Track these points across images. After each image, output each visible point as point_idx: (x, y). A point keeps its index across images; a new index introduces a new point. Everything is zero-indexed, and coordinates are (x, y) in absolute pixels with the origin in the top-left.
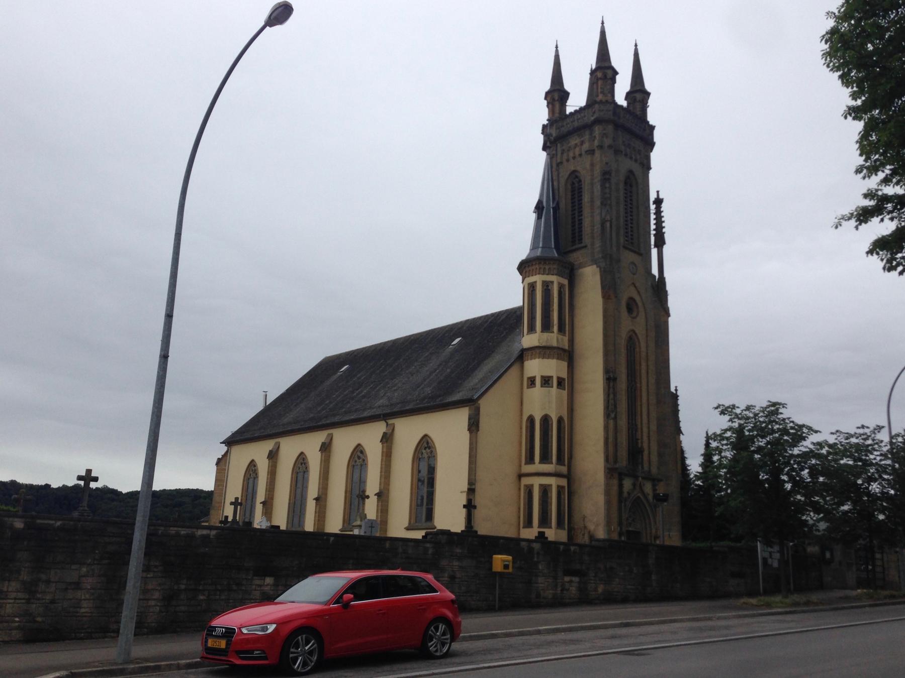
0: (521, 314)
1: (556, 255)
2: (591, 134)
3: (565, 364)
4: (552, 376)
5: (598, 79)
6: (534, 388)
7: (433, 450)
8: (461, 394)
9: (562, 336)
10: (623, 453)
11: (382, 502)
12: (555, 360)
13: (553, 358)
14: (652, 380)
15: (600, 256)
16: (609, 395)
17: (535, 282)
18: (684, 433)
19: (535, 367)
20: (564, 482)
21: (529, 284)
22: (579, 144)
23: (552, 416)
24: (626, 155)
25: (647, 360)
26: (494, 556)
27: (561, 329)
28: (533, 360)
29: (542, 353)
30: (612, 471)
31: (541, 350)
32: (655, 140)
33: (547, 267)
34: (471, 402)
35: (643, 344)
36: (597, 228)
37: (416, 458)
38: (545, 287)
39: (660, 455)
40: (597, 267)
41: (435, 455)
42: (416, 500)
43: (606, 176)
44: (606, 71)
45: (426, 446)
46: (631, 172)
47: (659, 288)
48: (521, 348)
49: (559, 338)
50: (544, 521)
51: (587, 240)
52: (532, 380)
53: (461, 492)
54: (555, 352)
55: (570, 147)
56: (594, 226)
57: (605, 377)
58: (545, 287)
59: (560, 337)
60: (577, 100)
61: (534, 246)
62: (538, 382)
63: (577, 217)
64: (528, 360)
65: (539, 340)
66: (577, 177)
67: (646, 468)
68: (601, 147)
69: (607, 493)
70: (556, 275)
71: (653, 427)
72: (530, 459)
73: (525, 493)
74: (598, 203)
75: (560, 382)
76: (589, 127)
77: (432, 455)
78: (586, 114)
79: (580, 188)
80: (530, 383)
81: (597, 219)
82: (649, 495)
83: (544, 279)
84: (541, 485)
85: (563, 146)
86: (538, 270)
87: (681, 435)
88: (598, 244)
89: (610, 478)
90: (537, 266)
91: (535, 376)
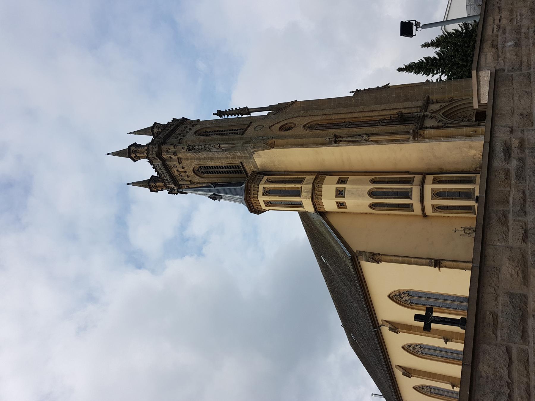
1: (244, 185)
4: (336, 188)
5: (137, 156)
10: (402, 128)
12: (323, 186)
14: (345, 110)
17: (264, 201)
20: (430, 178)
22: (176, 169)
24: (184, 136)
27: (300, 181)
28: (324, 204)
29: (317, 196)
30: (417, 136)
31: (315, 198)
33: (253, 192)
34: (355, 258)
35: (316, 118)
36: (226, 154)
38: (268, 193)
39: (406, 100)
40: (254, 154)
42: (438, 393)
43: (191, 148)
50: (467, 195)
51: (237, 163)
52: (340, 204)
54: (317, 187)
55: (180, 175)
57: (335, 145)
58: (268, 193)
59: (305, 182)
63: (212, 170)
66: (198, 170)
68: (175, 153)
69: (438, 138)
71: (383, 107)
72: (409, 207)
73: (440, 212)
75: (342, 181)
77: (408, 293)
84: (432, 198)
86: (255, 199)
88: (238, 154)
90: (252, 199)
91: (336, 202)
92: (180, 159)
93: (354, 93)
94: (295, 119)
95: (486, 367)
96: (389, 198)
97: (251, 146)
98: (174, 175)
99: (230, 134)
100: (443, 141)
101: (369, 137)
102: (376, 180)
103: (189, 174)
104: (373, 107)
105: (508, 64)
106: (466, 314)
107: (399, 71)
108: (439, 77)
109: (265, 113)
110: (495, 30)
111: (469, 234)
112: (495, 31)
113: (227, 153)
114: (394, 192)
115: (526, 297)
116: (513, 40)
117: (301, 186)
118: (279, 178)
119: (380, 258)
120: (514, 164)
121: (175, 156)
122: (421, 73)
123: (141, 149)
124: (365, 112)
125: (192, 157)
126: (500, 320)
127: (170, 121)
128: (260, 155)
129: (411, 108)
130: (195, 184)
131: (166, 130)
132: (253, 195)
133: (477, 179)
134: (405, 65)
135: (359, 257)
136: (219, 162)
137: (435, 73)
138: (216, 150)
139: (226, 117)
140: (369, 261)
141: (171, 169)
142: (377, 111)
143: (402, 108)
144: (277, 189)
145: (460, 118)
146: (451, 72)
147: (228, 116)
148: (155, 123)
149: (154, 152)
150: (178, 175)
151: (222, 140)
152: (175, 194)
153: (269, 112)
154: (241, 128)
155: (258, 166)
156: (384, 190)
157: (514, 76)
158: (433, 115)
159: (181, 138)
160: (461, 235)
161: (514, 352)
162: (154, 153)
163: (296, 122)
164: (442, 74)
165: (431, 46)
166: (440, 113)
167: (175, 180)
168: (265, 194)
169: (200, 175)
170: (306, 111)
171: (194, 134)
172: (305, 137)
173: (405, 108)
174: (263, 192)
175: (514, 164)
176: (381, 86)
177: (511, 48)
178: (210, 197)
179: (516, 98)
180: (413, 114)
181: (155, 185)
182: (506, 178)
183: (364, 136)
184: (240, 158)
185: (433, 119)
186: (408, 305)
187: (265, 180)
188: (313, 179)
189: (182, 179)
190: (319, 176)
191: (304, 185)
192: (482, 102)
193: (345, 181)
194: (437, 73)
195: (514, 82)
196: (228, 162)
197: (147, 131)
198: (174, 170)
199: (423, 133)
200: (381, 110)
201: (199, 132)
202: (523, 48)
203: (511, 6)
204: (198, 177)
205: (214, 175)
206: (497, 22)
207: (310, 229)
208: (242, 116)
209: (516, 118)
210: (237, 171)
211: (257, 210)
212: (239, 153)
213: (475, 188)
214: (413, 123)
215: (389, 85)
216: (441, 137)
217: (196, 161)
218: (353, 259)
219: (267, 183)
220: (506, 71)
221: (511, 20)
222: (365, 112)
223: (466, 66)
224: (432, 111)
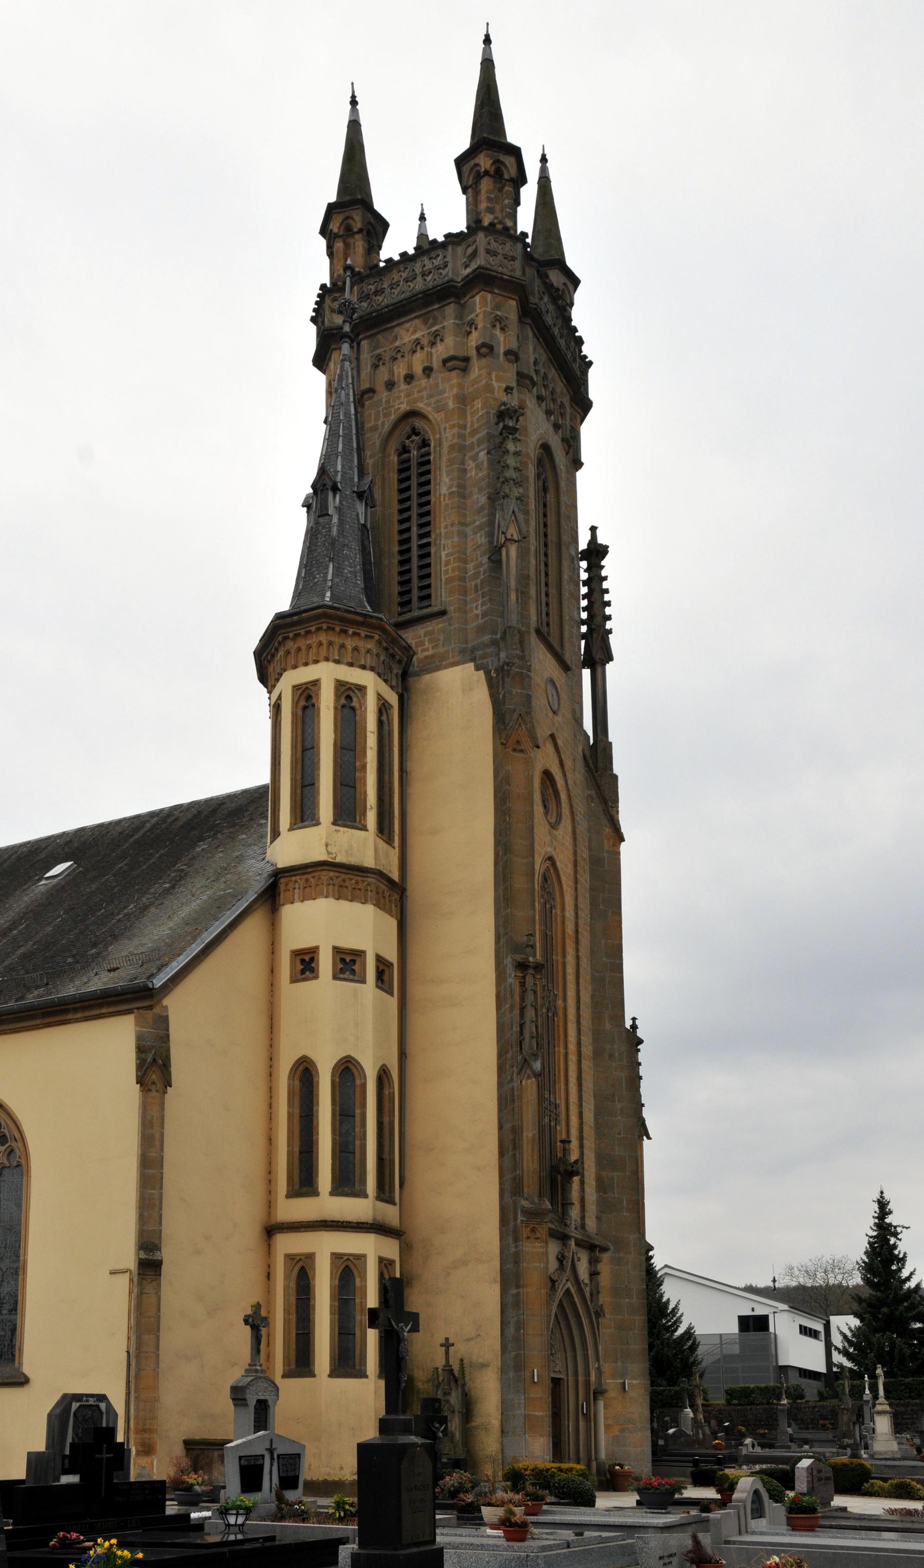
2: (460, 316)
5: (479, 177)
6: (313, 982)
7: (17, 1146)
12: (370, 909)
13: (365, 902)
17: (316, 683)
18: (651, 1134)
20: (390, 1248)
21: (296, 688)
22: (425, 341)
25: (577, 942)
26: (91, 1441)
28: (309, 903)
31: (332, 874)
32: (592, 395)
33: (350, 643)
40: (477, 668)
41: (23, 1162)
44: (503, 157)
48: (270, 869)
52: (307, 958)
53: (113, 1273)
58: (343, 701)
62: (325, 963)
63: (414, 529)
64: (292, 903)
66: (414, 431)
68: (486, 349)
70: (372, 669)
73: (287, 1277)
75: (383, 968)
78: (449, 259)
79: (425, 462)
83: (342, 677)
84: (336, 1257)
85: (376, 347)
87: (645, 1138)
91: (317, 948)
92: (462, 364)
94: (570, 828)
104: (588, 1085)
109: (588, 724)
113: (481, 565)
117: (368, 827)
118: (393, 751)
125: (469, 420)
127: (586, 350)
128: (471, 689)
132: (338, 640)
136: (446, 527)
141: (425, 322)
147: (585, 583)
150: (397, 344)
155: (427, 677)
156: (358, 1111)
166: (569, 1283)
169: (397, 432)
171: (544, 441)
174: (347, 683)
176: (645, 1113)
188: (390, 871)
190: (397, 894)
193: (382, 981)
204: (387, 427)
211: (277, 650)
212: (478, 612)
213: (367, 1377)
215: (645, 1138)
217: (455, 430)
218: (137, 995)
219: (378, 704)
224: (576, 1259)
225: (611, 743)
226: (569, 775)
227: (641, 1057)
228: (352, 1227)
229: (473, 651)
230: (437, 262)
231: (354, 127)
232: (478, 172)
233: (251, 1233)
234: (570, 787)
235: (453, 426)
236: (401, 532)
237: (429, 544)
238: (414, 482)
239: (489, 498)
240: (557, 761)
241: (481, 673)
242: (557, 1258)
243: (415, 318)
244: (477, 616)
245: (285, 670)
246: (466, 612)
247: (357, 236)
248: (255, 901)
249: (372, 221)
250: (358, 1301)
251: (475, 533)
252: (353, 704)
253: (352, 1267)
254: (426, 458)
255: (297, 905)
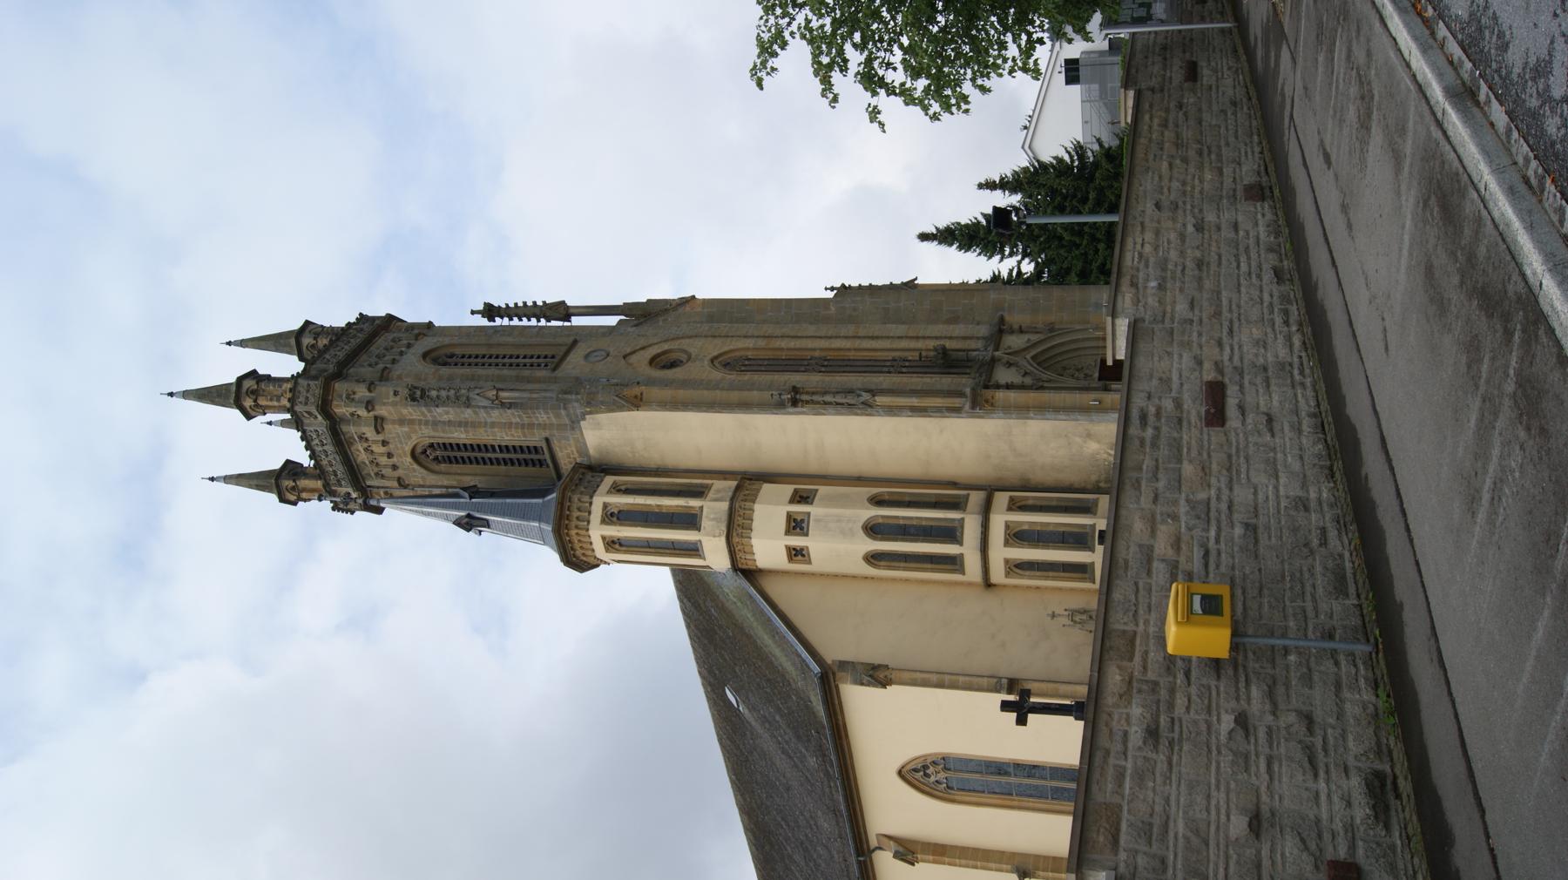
0: (683, 570)
1: (554, 495)
2: (348, 422)
3: (766, 487)
4: (788, 513)
5: (257, 406)
8: (812, 698)
9: (712, 491)
10: (946, 381)
11: (1038, 870)
12: (757, 507)
14: (811, 330)
15: (563, 412)
16: (825, 403)
17: (604, 538)
19: (768, 549)
20: (1001, 499)
22: (366, 445)
23: (868, 517)
24: (394, 361)
27: (699, 493)
28: (755, 550)
30: (979, 403)
31: (734, 534)
32: (383, 314)
33: (576, 514)
34: (828, 680)
35: (741, 344)
36: (512, 416)
37: (946, 795)
38: (615, 519)
39: (954, 320)
40: (584, 419)
43: (417, 395)
45: (922, 773)
46: (425, 355)
47: (642, 314)
49: (715, 496)
50: (1079, 540)
51: (535, 439)
52: (794, 552)
54: (740, 507)
56: (511, 423)
57: (791, 410)
58: (615, 519)
59: (711, 494)
60: (285, 446)
61: (270, 491)
62: (797, 541)
63: (489, 455)
64: (755, 560)
65: (714, 536)
66: (424, 452)
67: (980, 344)
68: (369, 405)
69: (1023, 411)
70: (591, 497)
71: (900, 329)
73: (1022, 577)
74: (468, 414)
75: (801, 498)
76: (334, 426)
77: (946, 762)
80: (800, 557)
81: (496, 415)
82: (1029, 340)
83: (599, 519)
84: (1007, 543)
85: (369, 475)
86: (580, 532)
87: (916, 282)
88: (542, 417)
89: (992, 405)
90: (573, 532)
91: (786, 546)
92: (379, 421)
93: (835, 291)
95: (1118, 595)
96: (912, 541)
97: (583, 399)
98: (355, 462)
99: (518, 365)
100: (1032, 419)
101: (874, 396)
102: (882, 498)
103: (401, 460)
104: (877, 329)
105: (1148, 313)
106: (1072, 809)
107: (922, 241)
108: (1016, 264)
109: (612, 321)
110: (1136, 260)
111: (1080, 623)
112: (1135, 262)
113: (513, 414)
114: (921, 526)
115: (1152, 546)
116: (1157, 279)
119: (889, 677)
120: (1150, 432)
121: (369, 411)
122: (975, 251)
123: (271, 387)
124: (859, 337)
125: (414, 417)
126: (1130, 564)
127: (353, 320)
128: (599, 424)
129: (965, 338)
130: (411, 487)
131: (343, 342)
133: (1100, 505)
134: (936, 228)
135: (839, 675)
137: (1007, 253)
138: (486, 403)
139: (506, 322)
140: (862, 684)
141: (352, 443)
142: (888, 337)
143: (946, 338)
144: (639, 508)
145: (1068, 371)
146: (1043, 256)
147: (511, 319)
148: (307, 323)
149: (310, 397)
150: (367, 463)
151: (502, 379)
152: (347, 513)
153: (621, 320)
154: (550, 353)
156: (901, 522)
157: (1155, 330)
158: (1013, 359)
159: (388, 366)
160: (1064, 626)
161: (1141, 585)
162: (312, 400)
163: (691, 350)
164: (1023, 259)
165: (1000, 189)
167: (355, 475)
168: (606, 519)
169: (424, 463)
170: (716, 325)
172: (716, 386)
173: (951, 338)
175: (1150, 432)
177: (1154, 291)
178: (458, 523)
179: (1156, 359)
180: (970, 353)
181: (294, 484)
182: (1141, 447)
183: (864, 394)
184: (544, 429)
185: (1013, 369)
186: (941, 794)
187: (609, 486)
189: (377, 474)
191: (709, 503)
192: (1118, 358)
193: (808, 497)
194: (1011, 255)
195: (1155, 338)
196: (513, 435)
197: (282, 341)
198: (359, 447)
199: (993, 398)
200: (899, 337)
201: (434, 355)
202: (1168, 293)
203: (1157, 225)
204: (422, 470)
205: (468, 468)
206: (1138, 247)
207: (704, 618)
208: (549, 324)
209: (1155, 382)
210: (532, 460)
211: (582, 560)
214: (969, 374)
215: (916, 282)
216: (1029, 407)
217: (423, 427)
220: (1147, 322)
221: (1156, 248)
222: (859, 337)
223: (1078, 246)
225: (624, 304)
226: (651, 342)
227: (855, 284)
228: (985, 531)
229: (573, 422)
230: (314, 436)
231: (228, 479)
232: (254, 406)
233: (990, 600)
234: (659, 340)
235: (421, 429)
236: (492, 464)
237: (499, 446)
238: (458, 454)
239: (468, 407)
240: (642, 352)
241: (587, 417)
242: (1008, 367)
243: (350, 450)
244: (548, 418)
245: (595, 557)
246: (545, 425)
247: (298, 483)
248: (755, 588)
249: (286, 472)
250: (1039, 528)
251: (491, 417)
252: (616, 512)
253: (1013, 532)
254: (441, 445)
255: (756, 557)
